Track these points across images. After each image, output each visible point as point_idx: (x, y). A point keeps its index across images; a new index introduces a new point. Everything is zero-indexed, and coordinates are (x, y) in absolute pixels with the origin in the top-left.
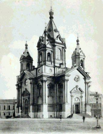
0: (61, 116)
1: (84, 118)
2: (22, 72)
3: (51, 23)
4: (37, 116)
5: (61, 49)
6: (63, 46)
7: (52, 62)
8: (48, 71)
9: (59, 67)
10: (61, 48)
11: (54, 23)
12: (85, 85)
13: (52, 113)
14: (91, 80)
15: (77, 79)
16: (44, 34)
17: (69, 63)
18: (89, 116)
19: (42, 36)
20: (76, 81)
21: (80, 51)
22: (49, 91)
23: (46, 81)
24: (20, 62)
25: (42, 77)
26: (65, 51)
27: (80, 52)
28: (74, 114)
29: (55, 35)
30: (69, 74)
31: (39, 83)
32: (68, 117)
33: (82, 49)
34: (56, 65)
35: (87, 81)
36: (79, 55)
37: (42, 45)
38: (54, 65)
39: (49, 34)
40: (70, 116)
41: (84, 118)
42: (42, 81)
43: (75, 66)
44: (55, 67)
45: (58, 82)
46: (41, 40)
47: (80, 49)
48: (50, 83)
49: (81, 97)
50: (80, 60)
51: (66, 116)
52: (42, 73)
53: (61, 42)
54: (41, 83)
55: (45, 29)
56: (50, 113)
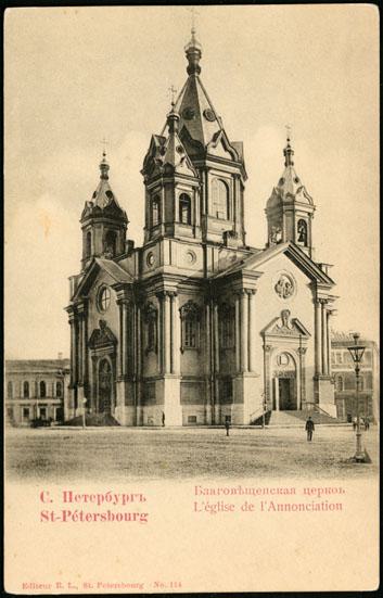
0: (228, 418)
1: (310, 426)
3: (191, 88)
4: (142, 419)
5: (228, 181)
6: (237, 171)
8: (181, 259)
9: (223, 246)
13: (194, 410)
14: (333, 291)
15: (284, 289)
16: (168, 127)
17: (256, 230)
18: (327, 420)
21: (296, 186)
26: (242, 188)
27: (295, 191)
28: (273, 412)
29: (209, 129)
32: (252, 424)
33: (303, 181)
34: (210, 237)
35: (322, 293)
36: (293, 202)
38: (204, 239)
40: (261, 418)
41: (310, 426)
42: (161, 296)
44: (205, 244)
45: (218, 297)
46: (156, 148)
49: (302, 351)
50: (297, 219)
51: (246, 420)
53: (229, 157)
54: (155, 300)
55: (173, 111)
56: (189, 407)
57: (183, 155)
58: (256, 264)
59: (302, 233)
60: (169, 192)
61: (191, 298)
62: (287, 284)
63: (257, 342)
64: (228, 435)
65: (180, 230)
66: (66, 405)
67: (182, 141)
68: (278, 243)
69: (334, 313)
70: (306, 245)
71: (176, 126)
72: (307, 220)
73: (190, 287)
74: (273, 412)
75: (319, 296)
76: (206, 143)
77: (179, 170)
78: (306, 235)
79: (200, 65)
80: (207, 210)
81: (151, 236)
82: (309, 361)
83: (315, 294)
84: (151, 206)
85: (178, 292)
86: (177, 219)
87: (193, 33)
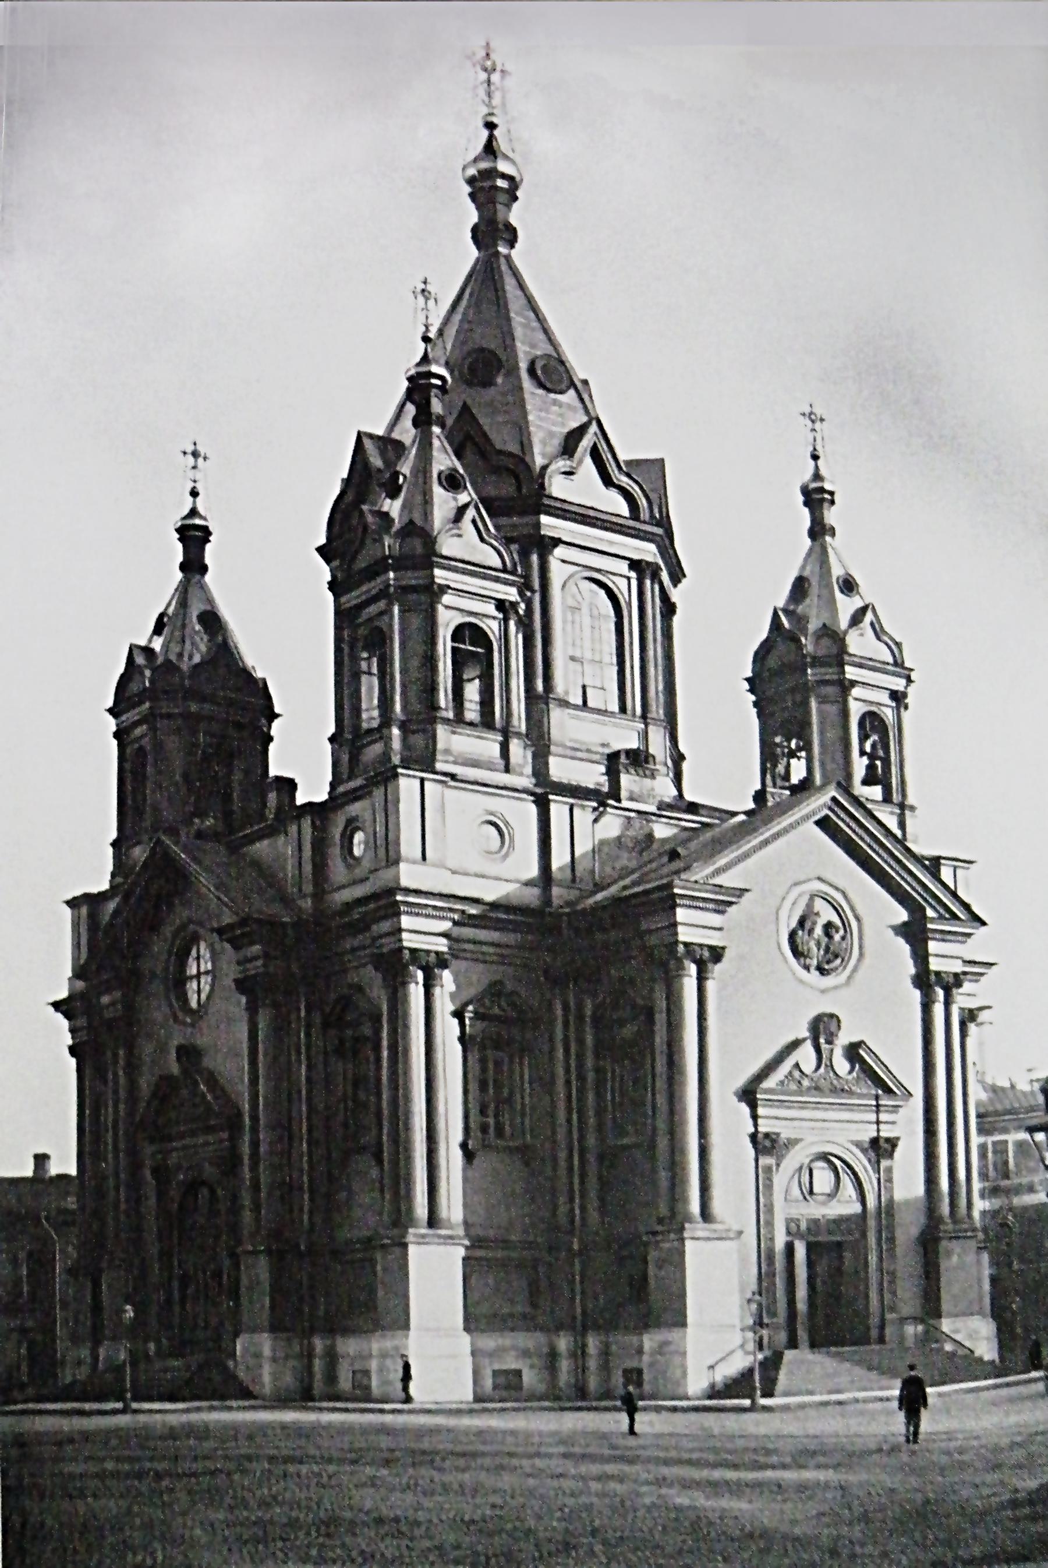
0: (634, 1376)
1: (913, 1401)
2: (139, 853)
3: (490, 281)
4: (331, 1377)
5: (620, 586)
6: (648, 552)
7: (506, 733)
8: (462, 842)
9: (603, 799)
10: (623, 567)
11: (521, 286)
13: (515, 1350)
14: (978, 946)
15: (820, 944)
16: (411, 409)
17: (721, 752)
18: (964, 1366)
19: (143, 642)
20: (816, 954)
21: (846, 606)
22: (483, 1085)
23: (442, 962)
24: (112, 724)
25: (394, 911)
26: (669, 609)
27: (844, 622)
28: (789, 1355)
29: (547, 418)
30: (725, 880)
31: (360, 989)
32: (714, 1393)
33: (868, 593)
34: (559, 769)
35: (944, 958)
36: (839, 656)
38: (540, 772)
40: (747, 1374)
41: (913, 1401)
42: (395, 965)
43: (805, 786)
44: (544, 792)
45: (592, 973)
46: (371, 472)
47: (849, 586)
48: (495, 990)
49: (881, 1148)
50: (856, 711)
51: (696, 1383)
52: (393, 860)
53: (624, 509)
54: (371, 979)
55: (425, 359)
56: (489, 1342)
57: (463, 498)
58: (722, 862)
59: (872, 757)
61: (496, 973)
63: (730, 1122)
64: (632, 1431)
65: (449, 741)
68: (795, 790)
69: (983, 1016)
70: (887, 799)
71: (437, 406)
72: (888, 714)
73: (494, 936)
74: (789, 1355)
75: (934, 964)
76: (539, 461)
77: (448, 546)
79: (513, 220)
80: (548, 678)
81: (354, 759)
82: (907, 1181)
83: (921, 957)
84: (355, 659)
85: (455, 953)
86: (444, 698)
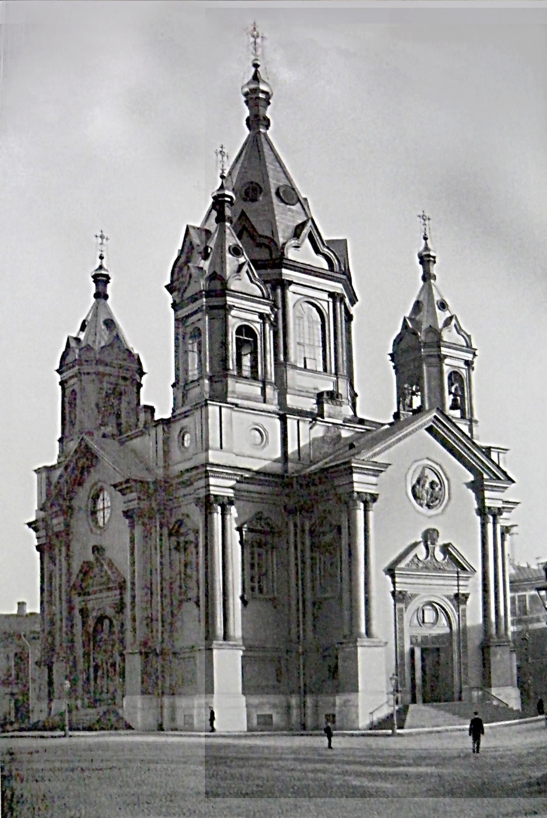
0: (331, 718)
1: (476, 730)
2: (73, 445)
3: (256, 147)
8: (243, 439)
9: (315, 417)
12: (484, 526)
13: (269, 705)
14: (511, 493)
15: (428, 493)
16: (214, 214)
17: (376, 392)
18: (504, 712)
19: (74, 335)
26: (349, 318)
28: (412, 707)
29: (285, 218)
30: (378, 459)
32: (372, 727)
34: (291, 401)
35: (492, 499)
36: (438, 343)
37: (202, 282)
38: (282, 403)
39: (243, 214)
41: (476, 730)
47: (443, 306)
49: (459, 599)
51: (363, 722)
53: (326, 266)
55: (222, 187)
56: (255, 700)
57: (242, 260)
60: (217, 324)
61: (259, 507)
62: (432, 483)
63: (381, 585)
64: (330, 747)
65: (237, 387)
66: (32, 695)
67: (240, 237)
68: (415, 412)
69: (514, 530)
70: (463, 417)
71: (228, 212)
72: (464, 372)
73: (258, 488)
74: (412, 707)
75: (488, 503)
76: (281, 240)
78: (463, 397)
79: (268, 115)
80: (286, 354)
82: (474, 616)
83: (481, 499)
85: (237, 497)
86: (232, 364)
87: (256, 66)
